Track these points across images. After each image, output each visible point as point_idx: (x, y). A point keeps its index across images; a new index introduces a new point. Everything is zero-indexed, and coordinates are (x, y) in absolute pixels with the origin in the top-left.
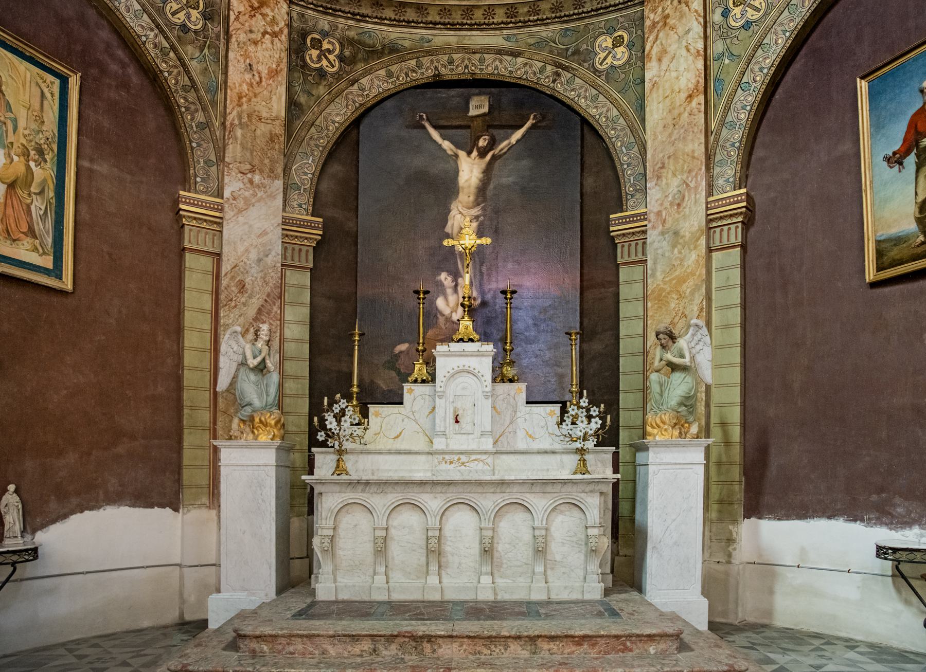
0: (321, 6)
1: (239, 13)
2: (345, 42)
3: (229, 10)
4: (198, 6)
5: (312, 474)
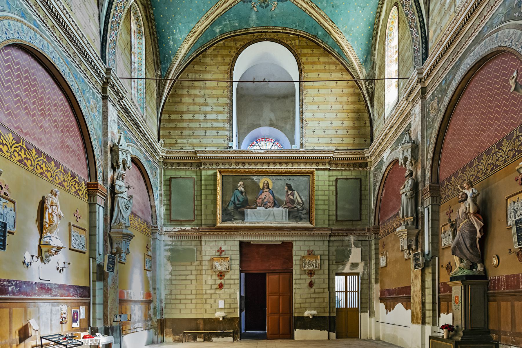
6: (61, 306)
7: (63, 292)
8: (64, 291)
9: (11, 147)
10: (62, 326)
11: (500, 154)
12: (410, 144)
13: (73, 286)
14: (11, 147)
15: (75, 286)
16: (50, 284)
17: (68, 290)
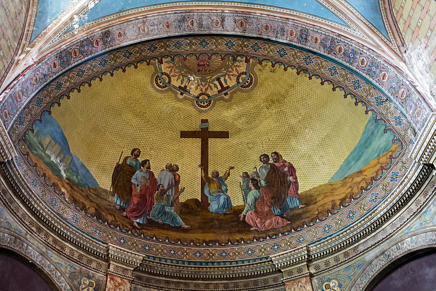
0: (144, 284)
1: (110, 288)
3: (106, 287)
4: (93, 286)
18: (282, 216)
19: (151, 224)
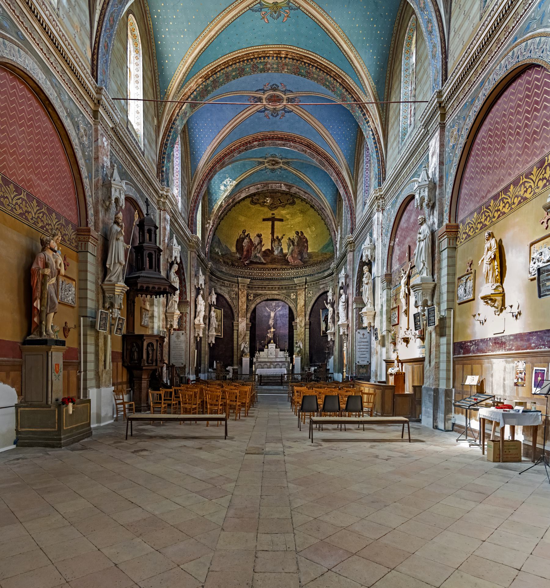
2: (254, 294)
5: (65, 346)
6: (516, 362)
7: (519, 343)
8: (522, 342)
9: (12, 200)
10: (517, 389)
11: (529, 184)
12: (428, 182)
13: (536, 332)
14: (12, 200)
15: (540, 331)
16: (504, 336)
17: (528, 340)
18: (301, 260)
19: (252, 263)
